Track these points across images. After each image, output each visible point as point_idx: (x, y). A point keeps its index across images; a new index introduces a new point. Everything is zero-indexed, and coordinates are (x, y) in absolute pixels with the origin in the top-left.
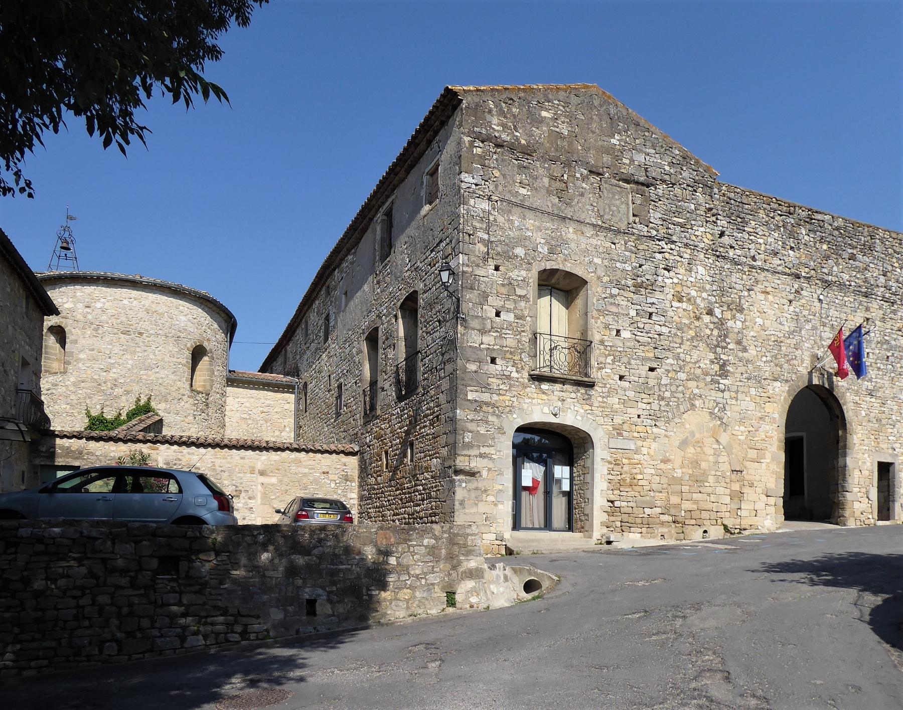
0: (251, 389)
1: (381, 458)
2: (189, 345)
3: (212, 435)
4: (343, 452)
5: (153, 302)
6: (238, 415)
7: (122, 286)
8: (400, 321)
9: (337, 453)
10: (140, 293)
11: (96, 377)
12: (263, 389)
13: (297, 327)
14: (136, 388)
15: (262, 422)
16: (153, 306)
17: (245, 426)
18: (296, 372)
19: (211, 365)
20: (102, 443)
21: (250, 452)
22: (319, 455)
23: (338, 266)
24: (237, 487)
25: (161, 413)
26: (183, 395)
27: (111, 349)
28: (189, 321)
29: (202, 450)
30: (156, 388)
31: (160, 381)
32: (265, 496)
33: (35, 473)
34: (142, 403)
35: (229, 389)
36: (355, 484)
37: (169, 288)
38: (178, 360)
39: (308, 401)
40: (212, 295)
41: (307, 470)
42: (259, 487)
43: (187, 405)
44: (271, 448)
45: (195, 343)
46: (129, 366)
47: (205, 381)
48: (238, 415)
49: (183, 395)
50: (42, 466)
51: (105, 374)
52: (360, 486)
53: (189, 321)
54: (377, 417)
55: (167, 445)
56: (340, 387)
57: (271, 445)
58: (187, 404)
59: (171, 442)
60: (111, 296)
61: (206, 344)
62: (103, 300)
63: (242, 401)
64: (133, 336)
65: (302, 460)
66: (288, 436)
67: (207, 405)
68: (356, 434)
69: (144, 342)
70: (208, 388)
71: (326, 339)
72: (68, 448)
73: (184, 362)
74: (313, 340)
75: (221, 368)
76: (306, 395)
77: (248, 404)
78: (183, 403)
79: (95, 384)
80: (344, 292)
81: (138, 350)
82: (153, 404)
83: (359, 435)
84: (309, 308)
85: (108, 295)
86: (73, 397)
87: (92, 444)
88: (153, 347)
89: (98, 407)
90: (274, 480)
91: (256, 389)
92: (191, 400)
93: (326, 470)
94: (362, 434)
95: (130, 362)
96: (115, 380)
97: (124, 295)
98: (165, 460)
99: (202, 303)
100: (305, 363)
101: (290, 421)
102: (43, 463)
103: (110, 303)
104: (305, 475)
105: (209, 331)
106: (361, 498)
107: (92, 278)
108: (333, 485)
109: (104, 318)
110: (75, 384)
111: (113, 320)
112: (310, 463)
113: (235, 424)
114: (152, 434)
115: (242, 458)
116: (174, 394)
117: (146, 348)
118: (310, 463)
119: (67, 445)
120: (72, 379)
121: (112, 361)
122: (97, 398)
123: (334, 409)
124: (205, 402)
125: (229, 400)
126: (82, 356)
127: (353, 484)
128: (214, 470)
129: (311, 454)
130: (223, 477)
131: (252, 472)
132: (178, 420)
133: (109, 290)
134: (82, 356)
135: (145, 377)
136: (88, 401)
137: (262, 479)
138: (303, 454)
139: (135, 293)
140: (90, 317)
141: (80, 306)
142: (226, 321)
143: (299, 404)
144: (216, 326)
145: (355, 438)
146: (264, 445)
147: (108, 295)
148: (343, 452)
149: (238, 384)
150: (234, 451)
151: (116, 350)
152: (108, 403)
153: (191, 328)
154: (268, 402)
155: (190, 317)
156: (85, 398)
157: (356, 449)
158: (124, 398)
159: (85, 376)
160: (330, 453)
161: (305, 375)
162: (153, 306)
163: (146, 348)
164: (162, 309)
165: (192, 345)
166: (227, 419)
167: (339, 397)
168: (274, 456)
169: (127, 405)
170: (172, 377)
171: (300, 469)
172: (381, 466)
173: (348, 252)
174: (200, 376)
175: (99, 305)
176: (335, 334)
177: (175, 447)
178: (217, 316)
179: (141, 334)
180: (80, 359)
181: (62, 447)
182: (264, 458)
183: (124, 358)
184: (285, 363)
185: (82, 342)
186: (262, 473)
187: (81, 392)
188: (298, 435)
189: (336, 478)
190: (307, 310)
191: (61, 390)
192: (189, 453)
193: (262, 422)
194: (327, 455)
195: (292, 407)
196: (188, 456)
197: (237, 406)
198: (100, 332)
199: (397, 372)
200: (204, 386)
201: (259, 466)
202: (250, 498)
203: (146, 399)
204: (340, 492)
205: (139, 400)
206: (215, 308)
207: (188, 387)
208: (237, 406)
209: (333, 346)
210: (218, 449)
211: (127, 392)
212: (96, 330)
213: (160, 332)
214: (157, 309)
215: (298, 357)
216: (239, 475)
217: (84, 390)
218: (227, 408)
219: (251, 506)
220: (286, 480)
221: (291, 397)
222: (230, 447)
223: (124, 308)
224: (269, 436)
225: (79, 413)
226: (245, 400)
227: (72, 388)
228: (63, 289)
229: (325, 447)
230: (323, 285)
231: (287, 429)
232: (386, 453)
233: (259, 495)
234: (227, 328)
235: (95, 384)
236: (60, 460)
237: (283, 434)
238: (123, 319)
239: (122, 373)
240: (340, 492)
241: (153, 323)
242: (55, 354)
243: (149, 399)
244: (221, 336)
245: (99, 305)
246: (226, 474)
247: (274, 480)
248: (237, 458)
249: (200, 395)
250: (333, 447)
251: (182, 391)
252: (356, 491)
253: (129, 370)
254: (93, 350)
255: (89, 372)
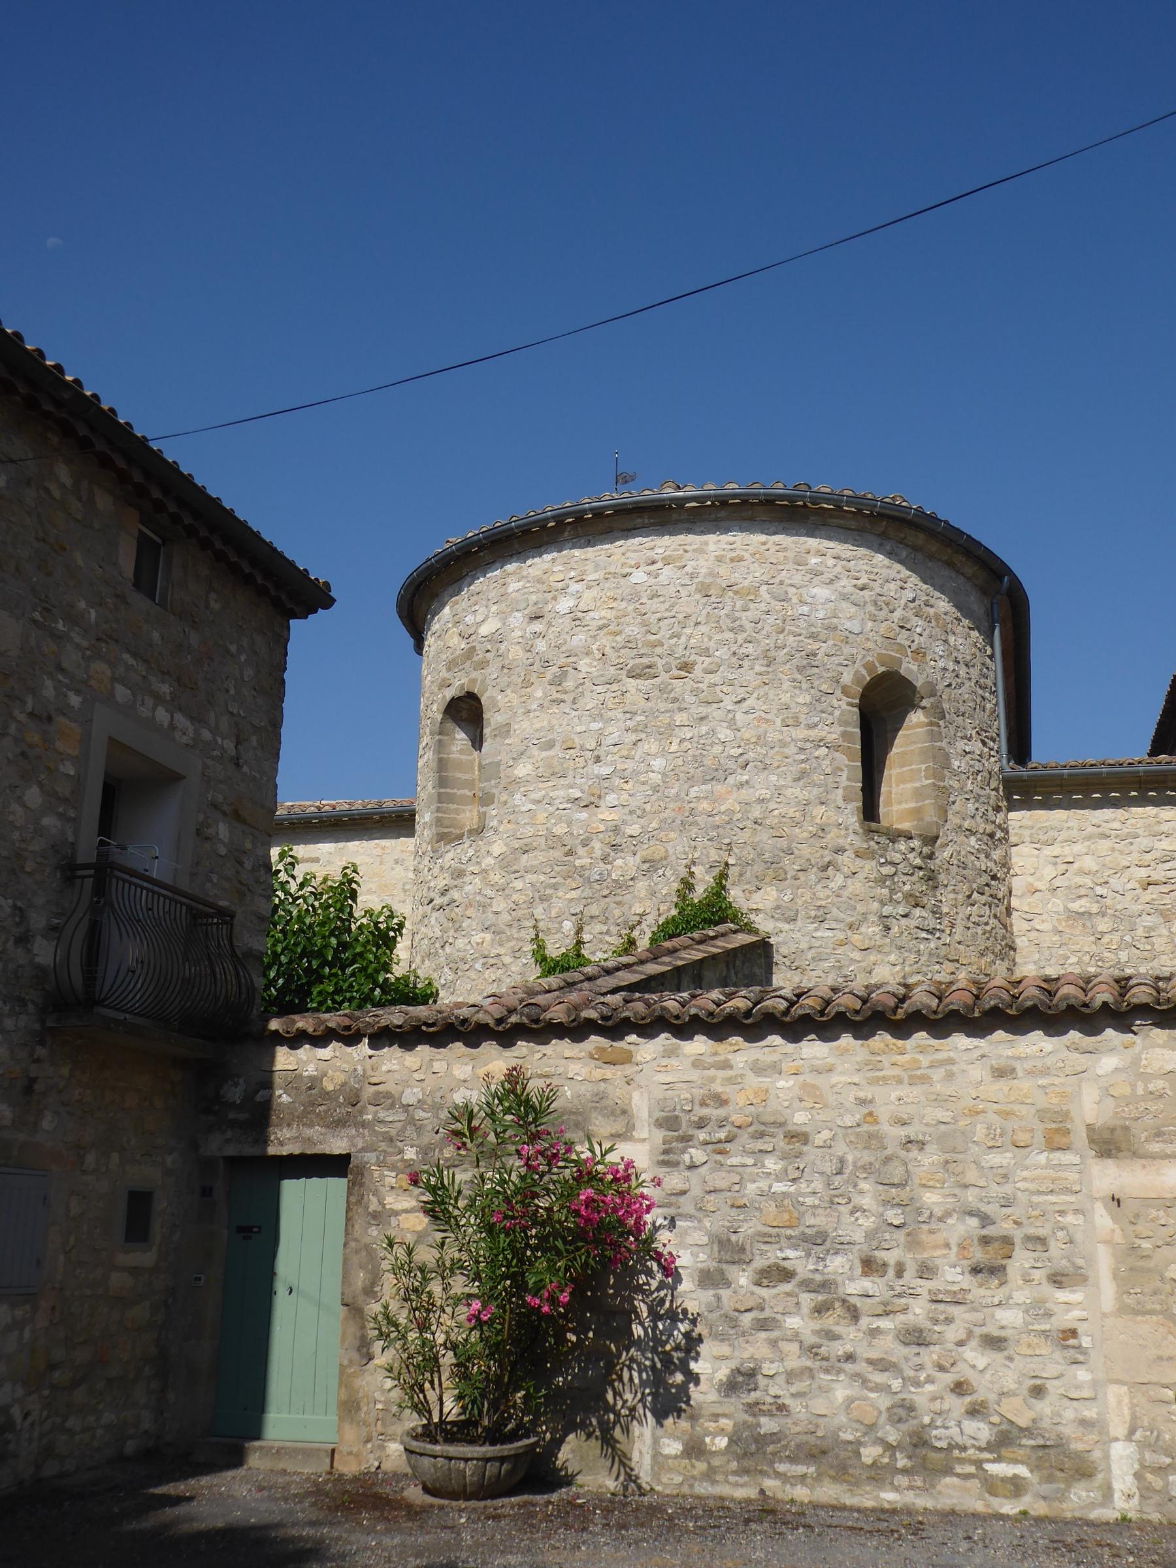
0: (1097, 805)
2: (847, 678)
3: (962, 972)
5: (719, 560)
6: (1057, 903)
7: (629, 532)
11: (560, 829)
12: (1143, 801)
14: (677, 847)
15: (1148, 921)
16: (723, 570)
17: (1086, 943)
19: (935, 736)
21: (1036, 1043)
24: (986, 1220)
25: (764, 924)
26: (839, 851)
27: (600, 733)
28: (845, 597)
29: (813, 1049)
30: (744, 836)
31: (756, 812)
33: (207, 1192)
34: (699, 893)
37: (768, 502)
38: (814, 734)
42: (1103, 1219)
43: (856, 886)
45: (869, 667)
46: (655, 778)
47: (918, 794)
48: (1057, 903)
49: (839, 851)
50: (231, 1161)
51: (584, 815)
53: (845, 597)
55: (664, 1040)
57: (1141, 995)
58: (856, 880)
59: (803, 1022)
60: (597, 567)
61: (909, 668)
62: (574, 587)
63: (1068, 852)
64: (664, 677)
67: (931, 878)
69: (696, 692)
70: (931, 816)
72: (314, 1083)
73: (833, 734)
75: (977, 747)
77: (1089, 863)
78: (839, 880)
79: (558, 854)
81: (680, 718)
82: (735, 895)
85: (590, 567)
86: (500, 904)
88: (728, 703)
89: (568, 926)
91: (1115, 804)
92: (869, 866)
95: (658, 763)
96: (616, 830)
97: (633, 557)
98: (661, 1104)
99: (883, 535)
102: (231, 1151)
103: (594, 592)
105: (918, 624)
110: (506, 864)
111: (605, 641)
113: (1049, 939)
114: (715, 994)
115: (1002, 1073)
117: (703, 710)
119: (310, 1070)
120: (498, 848)
121: (605, 770)
122: (565, 898)
124: (923, 870)
125: (1022, 857)
126: (523, 770)
128: (873, 1140)
130: (919, 1175)
131: (1057, 1140)
132: (823, 938)
133: (590, 552)
134: (523, 770)
135: (705, 805)
136: (539, 911)
137: (1108, 1176)
139: (664, 544)
140: (541, 645)
142: (983, 591)
144: (943, 605)
147: (590, 567)
149: (1047, 795)
150: (960, 1041)
151: (614, 733)
152: (594, 910)
153: (851, 620)
156: (531, 903)
158: (641, 886)
159: (529, 831)
162: (723, 570)
163: (703, 710)
165: (857, 678)
166: (1018, 923)
169: (650, 904)
170: (796, 792)
174: (902, 780)
175: (565, 604)
177: (700, 1045)
178: (945, 572)
179: (687, 667)
180: (516, 781)
181: (294, 1080)
182: (1108, 1063)
183: (638, 753)
185: (523, 726)
186: (1109, 1144)
187: (518, 884)
191: (472, 886)
192: (758, 1069)
193: (1148, 921)
196: (754, 1081)
197: (1049, 872)
198: (569, 684)
200: (917, 813)
201: (1090, 1108)
202: (1058, 1280)
203: (710, 879)
206: (934, 547)
207: (851, 816)
208: (1049, 872)
210: (882, 1039)
211: (652, 865)
212: (557, 682)
213: (750, 649)
214: (736, 577)
216: (994, 1159)
217: (530, 877)
218: (1017, 884)
219: (1068, 1319)
225: (516, 953)
226: (1078, 848)
227: (496, 878)
228: (480, 584)
233: (1104, 1264)
234: (990, 613)
235: (558, 854)
238: (633, 630)
239: (634, 803)
241: (726, 623)
242: (470, 784)
243: (723, 876)
245: (565, 604)
246: (930, 1158)
248: (978, 1072)
249: (902, 846)
253: (656, 789)
254: (550, 745)
255: (541, 817)
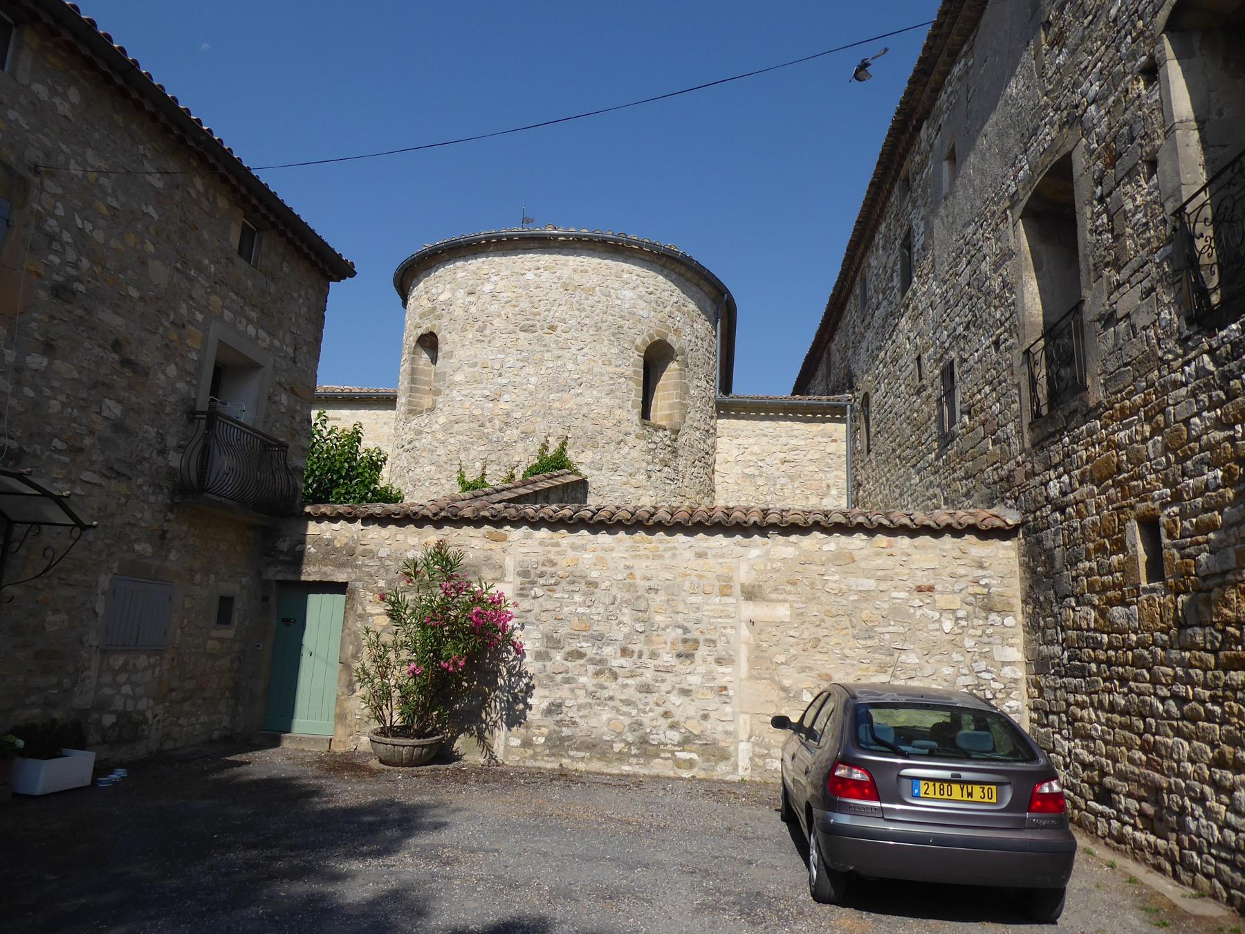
1: (1121, 546)
2: (638, 341)
4: (973, 529)
5: (575, 270)
6: (738, 469)
7: (526, 250)
8: (1174, 71)
9: (957, 532)
10: (555, 256)
11: (477, 412)
12: (785, 419)
13: (847, 298)
14: (541, 426)
15: (783, 480)
18: (849, 383)
19: (682, 377)
20: (392, 528)
21: (719, 540)
22: (904, 542)
23: (926, 114)
24: (686, 630)
25: (584, 471)
27: (503, 360)
28: (641, 297)
29: (604, 538)
30: (577, 423)
31: (585, 410)
32: (759, 656)
34: (551, 452)
35: (721, 422)
36: (1015, 621)
37: (604, 241)
38: (618, 370)
39: (872, 430)
40: (681, 246)
41: (870, 584)
42: (745, 631)
43: (635, 453)
44: (773, 526)
45: (651, 336)
46: (531, 387)
47: (671, 407)
48: (738, 469)
51: (491, 405)
52: (1033, 626)
54: (1091, 413)
55: (525, 529)
56: (948, 374)
57: (773, 518)
58: (635, 451)
61: (672, 339)
62: (494, 278)
63: (745, 442)
65: (857, 554)
66: (836, 501)
67: (674, 452)
68: (1009, 478)
69: (557, 342)
70: (677, 419)
71: (906, 282)
72: (329, 542)
73: (629, 371)
74: (879, 304)
76: (867, 421)
77: (756, 449)
78: (626, 450)
79: (475, 425)
80: (946, 151)
81: (547, 356)
82: (570, 454)
83: (1019, 476)
84: (867, 248)
85: (503, 268)
86: (441, 451)
87: (374, 532)
89: (478, 465)
90: (782, 612)
91: (771, 419)
93: (925, 583)
94: (1030, 475)
96: (508, 414)
98: (521, 564)
99: (664, 266)
100: (864, 356)
101: (839, 477)
102: (280, 577)
103: (505, 282)
104: (866, 596)
105: (678, 316)
106: (1039, 665)
107: (478, 241)
108: (948, 625)
109: (494, 308)
110: (445, 429)
111: (509, 310)
112: (879, 562)
114: (554, 507)
115: (700, 555)
116: (609, 433)
117: (560, 352)
118: (879, 562)
119: (327, 535)
120: (442, 420)
121: (504, 381)
122: (478, 450)
123: (934, 428)
125: (723, 444)
126: (458, 377)
127: (1009, 621)
128: (632, 587)
129: (881, 540)
131: (725, 591)
134: (458, 377)
135: (557, 404)
136: (462, 456)
137: (750, 610)
138: (859, 540)
139: (545, 259)
140: (473, 309)
141: (461, 293)
142: (714, 301)
143: (855, 440)
144: (692, 306)
145: (1004, 488)
146: (754, 518)
147: (503, 268)
148: (973, 529)
150: (680, 537)
152: (493, 457)
153: (643, 310)
154: (794, 442)
155: (642, 290)
157: (1012, 518)
158: (520, 446)
159: (460, 412)
160: (936, 532)
161: (865, 382)
163: (560, 352)
164: (591, 280)
165: (644, 341)
166: (717, 477)
167: (949, 393)
168: (782, 548)
169: (524, 456)
170: (607, 401)
171: (851, 580)
172: (1128, 568)
173: (953, 58)
175: (488, 287)
176: (926, 265)
177: (544, 533)
178: (695, 289)
179: (553, 328)
180: (454, 384)
181: (318, 541)
182: (754, 553)
183: (523, 373)
184: (829, 371)
185: (460, 354)
186: (751, 594)
187: (452, 441)
188: (855, 502)
189: (956, 601)
190: (863, 255)
191: (426, 440)
192: (574, 547)
193: (783, 480)
194: (926, 540)
195: (842, 447)
196: (571, 554)
197: (735, 452)
198: (487, 332)
199: (1182, 236)
200: (670, 417)
201: (744, 575)
202: (720, 661)
204: (969, 643)
205: (546, 448)
206: (689, 275)
207: (635, 416)
208: (735, 452)
209: (926, 288)
210: (640, 535)
212: (481, 330)
213: (587, 321)
214: (583, 281)
215: (850, 353)
216: (693, 599)
217: (458, 437)
218: (719, 458)
219: (723, 681)
220: (814, 610)
221: (840, 430)
222: (673, 528)
223: (526, 287)
224: (797, 501)
225: (449, 478)
226: (751, 441)
229: (920, 517)
230: (895, 180)
231: (834, 492)
232: (1150, 525)
233: (743, 654)
234: (716, 314)
235: (475, 425)
236: (311, 569)
237: (825, 502)
238: (525, 305)
239: (519, 401)
240: (969, 643)
241: (575, 306)
244: (703, 326)
245: (488, 287)
246: (660, 598)
247: (782, 612)
248: (688, 554)
249: (661, 433)
250: (942, 516)
251: (625, 427)
252: (1020, 639)
254: (475, 365)
255: (467, 404)
